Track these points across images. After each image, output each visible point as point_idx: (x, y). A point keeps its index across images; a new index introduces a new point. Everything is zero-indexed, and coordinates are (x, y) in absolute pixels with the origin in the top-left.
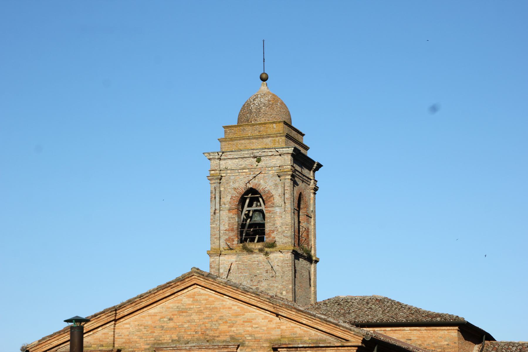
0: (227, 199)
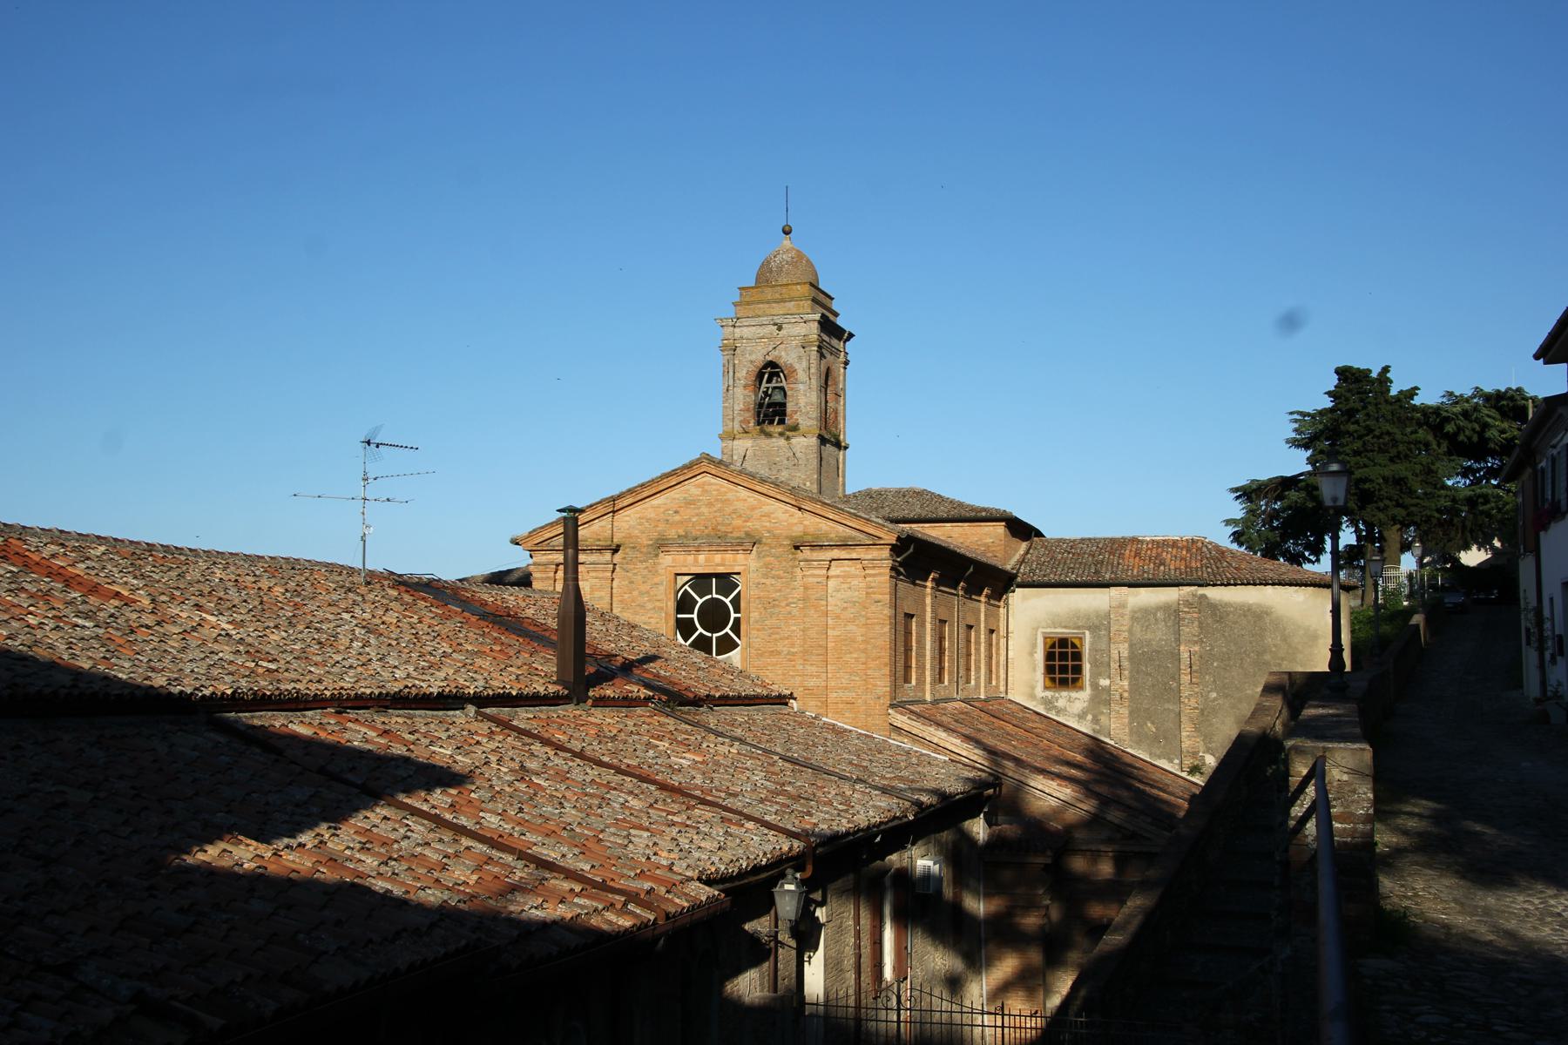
0: (742, 373)
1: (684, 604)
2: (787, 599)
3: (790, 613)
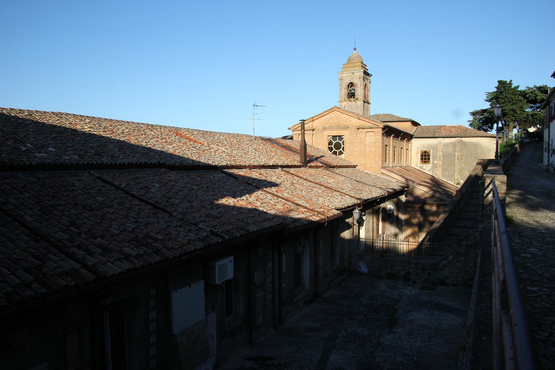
0: (344, 86)
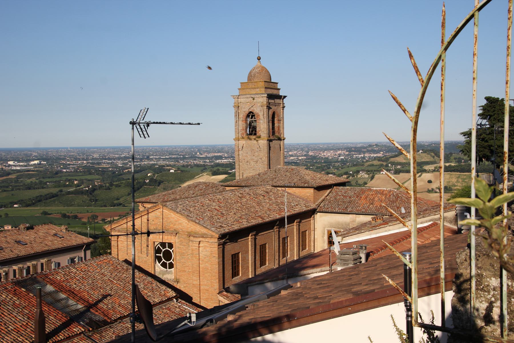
0: (241, 116)
1: (158, 251)
2: (187, 253)
3: (188, 258)
